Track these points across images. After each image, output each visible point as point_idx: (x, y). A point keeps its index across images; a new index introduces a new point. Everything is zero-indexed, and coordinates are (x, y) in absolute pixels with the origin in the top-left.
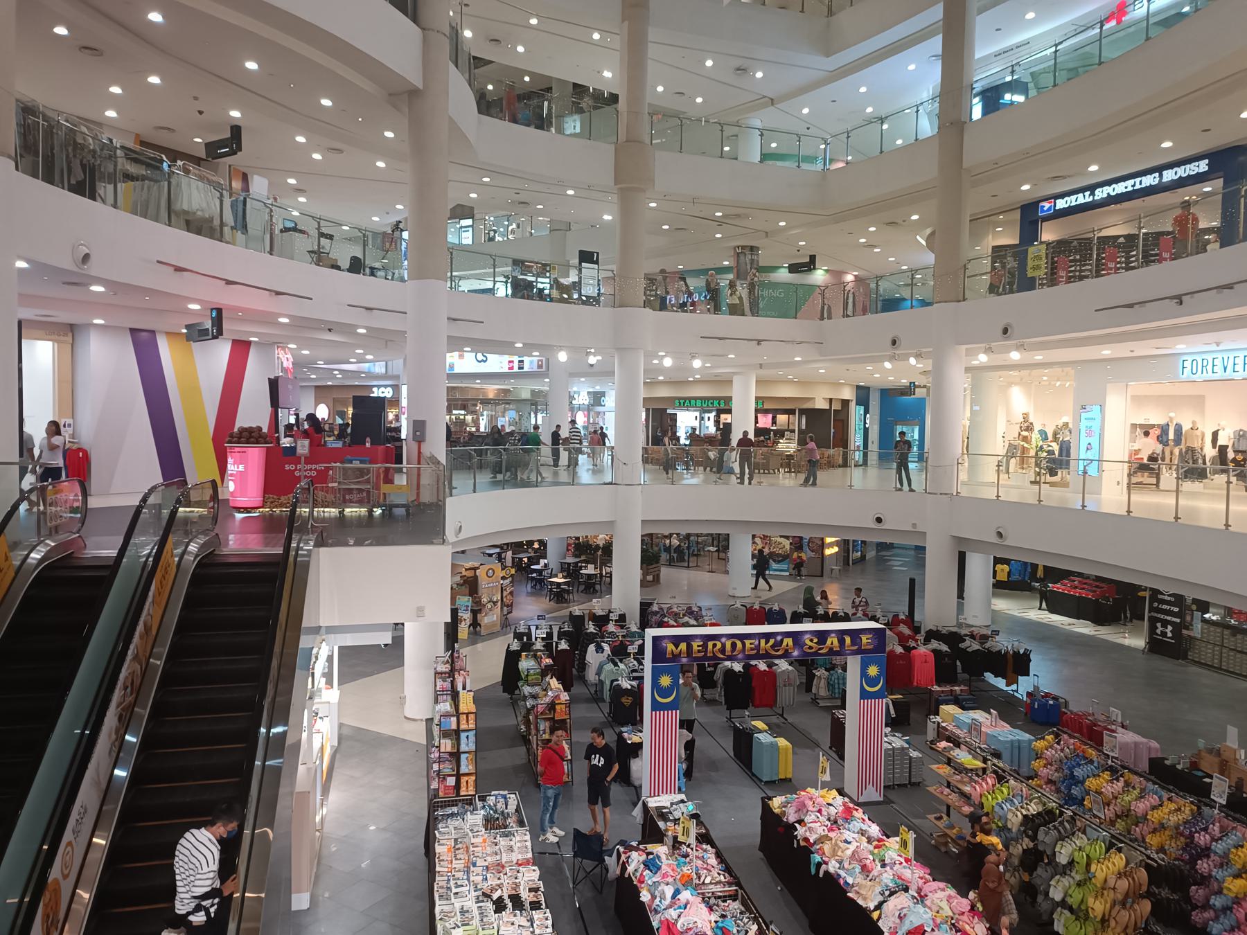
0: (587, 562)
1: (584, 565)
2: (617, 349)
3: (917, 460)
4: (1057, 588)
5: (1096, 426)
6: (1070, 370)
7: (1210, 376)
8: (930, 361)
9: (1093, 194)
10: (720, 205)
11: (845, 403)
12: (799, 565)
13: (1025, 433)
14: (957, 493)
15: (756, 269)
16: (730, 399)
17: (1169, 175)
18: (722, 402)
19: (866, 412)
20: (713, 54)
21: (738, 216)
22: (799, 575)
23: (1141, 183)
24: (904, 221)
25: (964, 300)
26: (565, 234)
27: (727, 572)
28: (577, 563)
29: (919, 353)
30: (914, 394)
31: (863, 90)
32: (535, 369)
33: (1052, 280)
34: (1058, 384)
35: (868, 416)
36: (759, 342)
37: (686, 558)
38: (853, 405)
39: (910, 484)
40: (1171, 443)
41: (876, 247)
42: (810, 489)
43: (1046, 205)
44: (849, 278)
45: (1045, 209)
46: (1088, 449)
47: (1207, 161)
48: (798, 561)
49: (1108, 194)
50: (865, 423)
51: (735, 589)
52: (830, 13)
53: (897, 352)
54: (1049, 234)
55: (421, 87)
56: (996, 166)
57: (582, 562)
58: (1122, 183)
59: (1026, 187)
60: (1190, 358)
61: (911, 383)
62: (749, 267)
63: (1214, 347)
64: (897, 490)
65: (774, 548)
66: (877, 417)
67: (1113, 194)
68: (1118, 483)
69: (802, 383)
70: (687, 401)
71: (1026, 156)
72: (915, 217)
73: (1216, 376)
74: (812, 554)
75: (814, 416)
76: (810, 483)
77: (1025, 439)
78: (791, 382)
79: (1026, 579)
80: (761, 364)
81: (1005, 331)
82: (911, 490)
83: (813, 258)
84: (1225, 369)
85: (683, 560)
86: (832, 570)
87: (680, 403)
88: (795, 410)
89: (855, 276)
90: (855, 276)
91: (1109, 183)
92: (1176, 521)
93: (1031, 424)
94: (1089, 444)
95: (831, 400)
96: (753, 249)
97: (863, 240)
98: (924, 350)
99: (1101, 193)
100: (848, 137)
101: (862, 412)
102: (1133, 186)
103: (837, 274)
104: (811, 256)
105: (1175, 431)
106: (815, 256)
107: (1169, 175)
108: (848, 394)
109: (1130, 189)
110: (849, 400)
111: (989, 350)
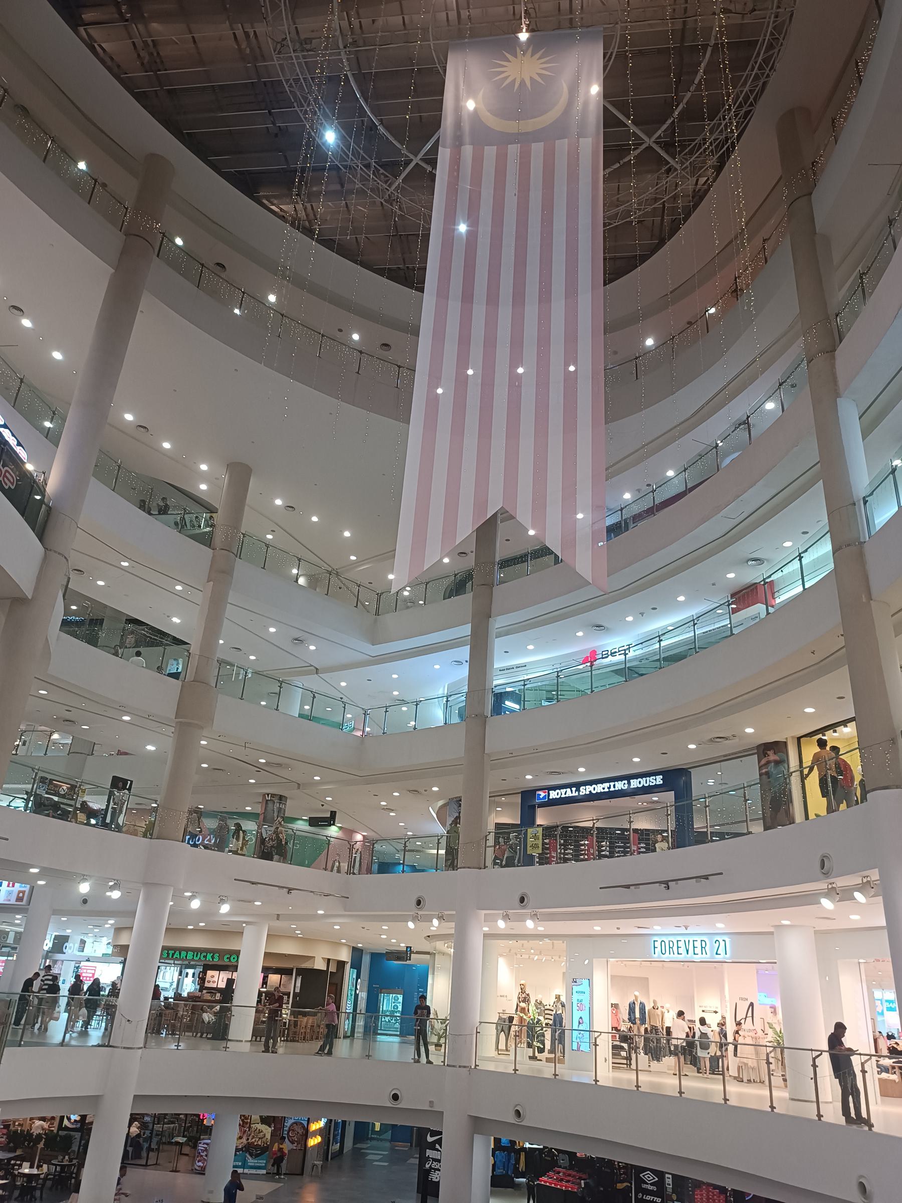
0: (23, 1159)
1: (18, 1162)
2: (146, 884)
3: (398, 1033)
4: (545, 1182)
5: (585, 999)
6: (560, 944)
7: (676, 957)
8: (453, 924)
9: (578, 790)
10: (265, 752)
11: (341, 964)
12: (278, 1160)
13: (523, 1005)
14: (476, 1065)
15: (282, 817)
16: (237, 953)
17: (635, 783)
18: (216, 956)
19: (358, 977)
20: (276, 622)
21: (279, 765)
22: (278, 1173)
23: (614, 787)
24: (425, 791)
25: (485, 868)
26: (86, 758)
27: (202, 1172)
28: (9, 1160)
29: (440, 915)
30: (410, 960)
31: (395, 676)
32: (13, 901)
33: (544, 860)
34: (536, 958)
35: (359, 980)
36: (290, 890)
37: (144, 1154)
38: (348, 967)
39: (427, 1056)
40: (638, 1022)
41: (392, 810)
42: (325, 1059)
43: (542, 794)
44: (359, 837)
45: (541, 797)
46: (579, 1023)
47: (661, 777)
48: (279, 1154)
49: (590, 792)
50: (356, 988)
51: (211, 1192)
52: (377, 614)
53: (420, 913)
54: (542, 818)
55: (30, 598)
56: (511, 755)
57: (16, 1158)
58: (601, 785)
59: (529, 777)
60: (659, 939)
61: (407, 947)
62: (275, 815)
63: (683, 930)
64: (415, 1062)
65: (253, 1137)
66: (366, 984)
67: (594, 792)
68: (606, 1060)
69: (306, 940)
70: (177, 953)
71: (535, 751)
72: (435, 789)
73: (680, 958)
74: (294, 1146)
75: (310, 976)
76: (326, 1051)
77: (523, 1010)
78: (296, 938)
79: (509, 1173)
80: (278, 915)
81: (522, 900)
82: (429, 1062)
83: (333, 814)
84: (687, 951)
85: (140, 1157)
86: (314, 1165)
87: (168, 954)
88: (292, 970)
89: (364, 836)
90: (364, 836)
91: (591, 783)
92: (681, 1096)
93: (528, 995)
94: (581, 1018)
95: (329, 960)
96: (281, 798)
97: (383, 803)
98: (446, 913)
99: (585, 790)
100: (386, 711)
101: (355, 977)
102: (609, 788)
103: (349, 832)
104: (332, 812)
105: (640, 1009)
106: (335, 812)
107: (635, 783)
108: (344, 955)
109: (606, 790)
110: (345, 962)
111: (506, 917)
